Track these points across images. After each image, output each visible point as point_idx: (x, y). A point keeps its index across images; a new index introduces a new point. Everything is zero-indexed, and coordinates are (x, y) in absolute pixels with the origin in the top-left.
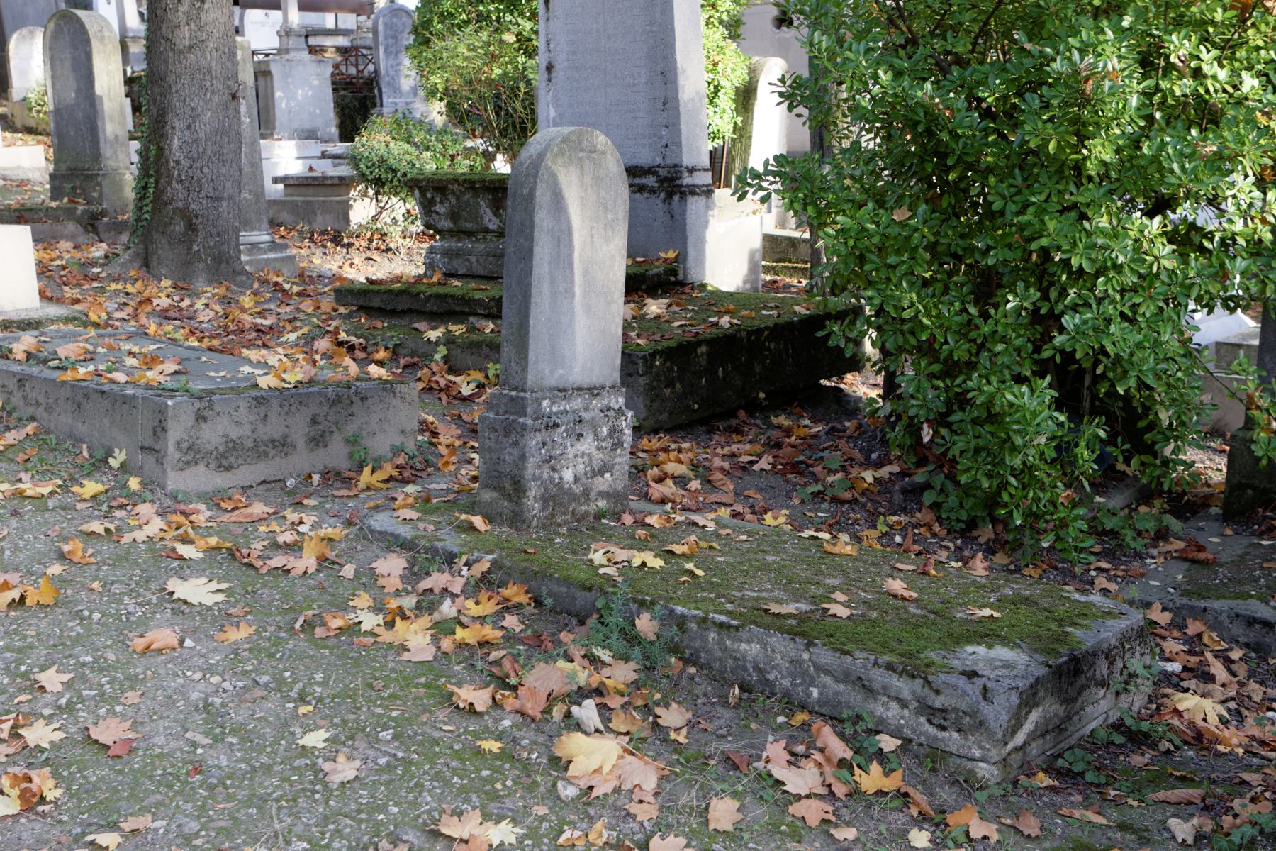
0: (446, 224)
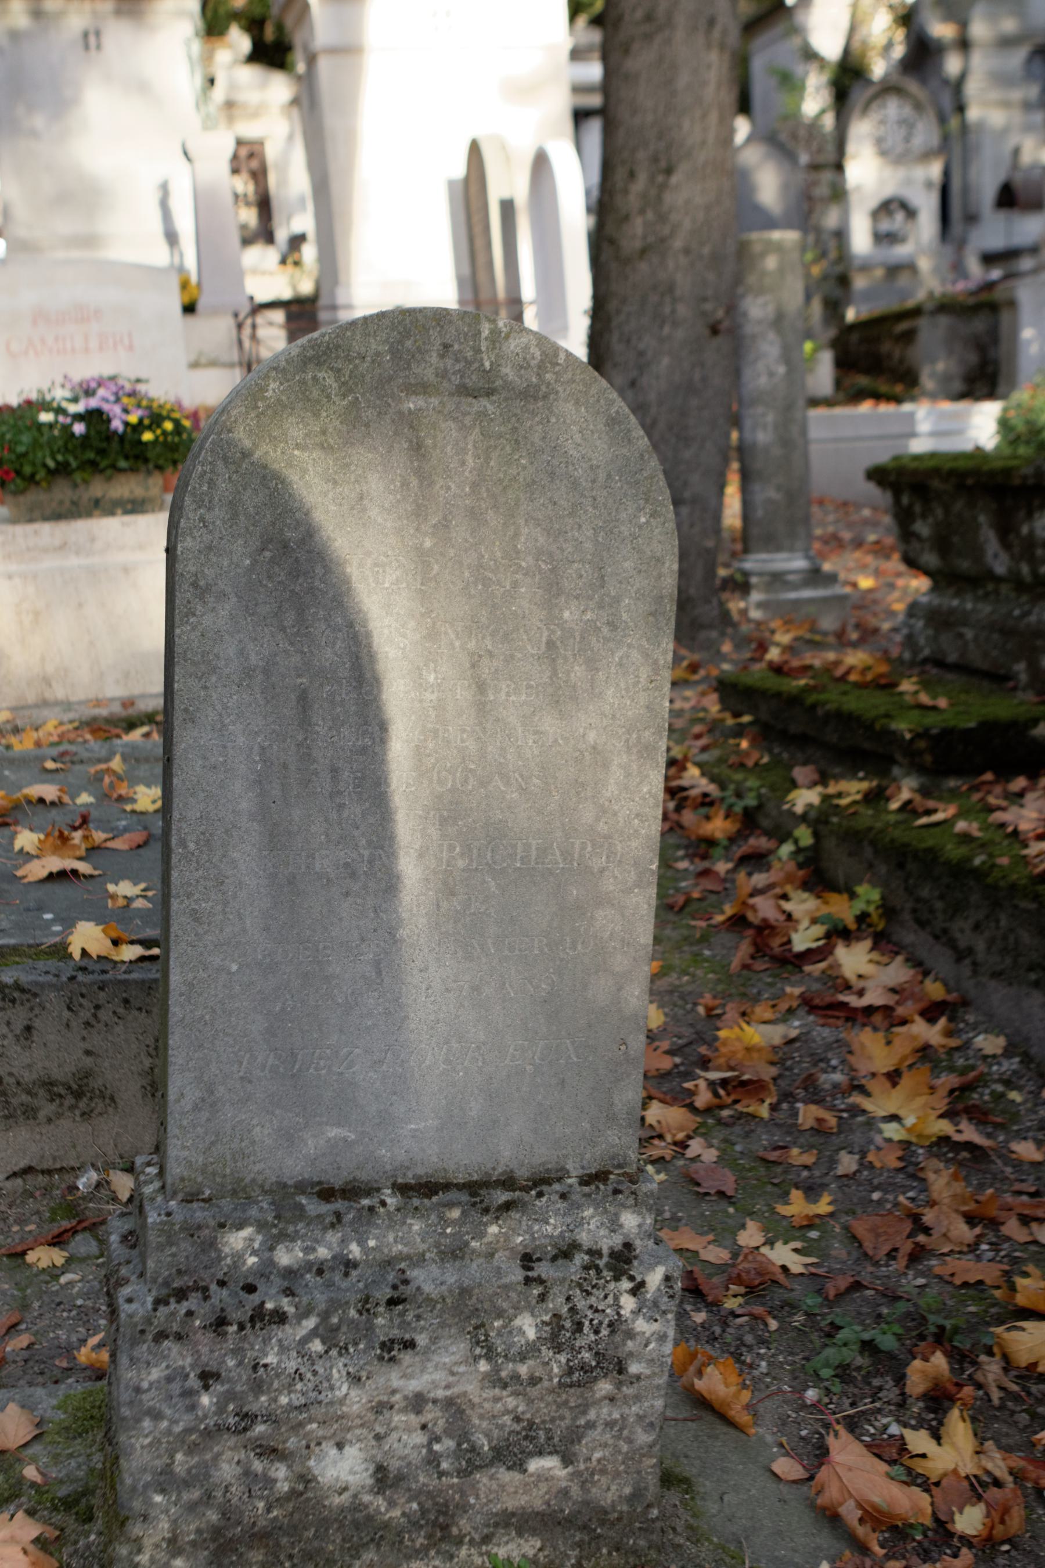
0: (931, 559)
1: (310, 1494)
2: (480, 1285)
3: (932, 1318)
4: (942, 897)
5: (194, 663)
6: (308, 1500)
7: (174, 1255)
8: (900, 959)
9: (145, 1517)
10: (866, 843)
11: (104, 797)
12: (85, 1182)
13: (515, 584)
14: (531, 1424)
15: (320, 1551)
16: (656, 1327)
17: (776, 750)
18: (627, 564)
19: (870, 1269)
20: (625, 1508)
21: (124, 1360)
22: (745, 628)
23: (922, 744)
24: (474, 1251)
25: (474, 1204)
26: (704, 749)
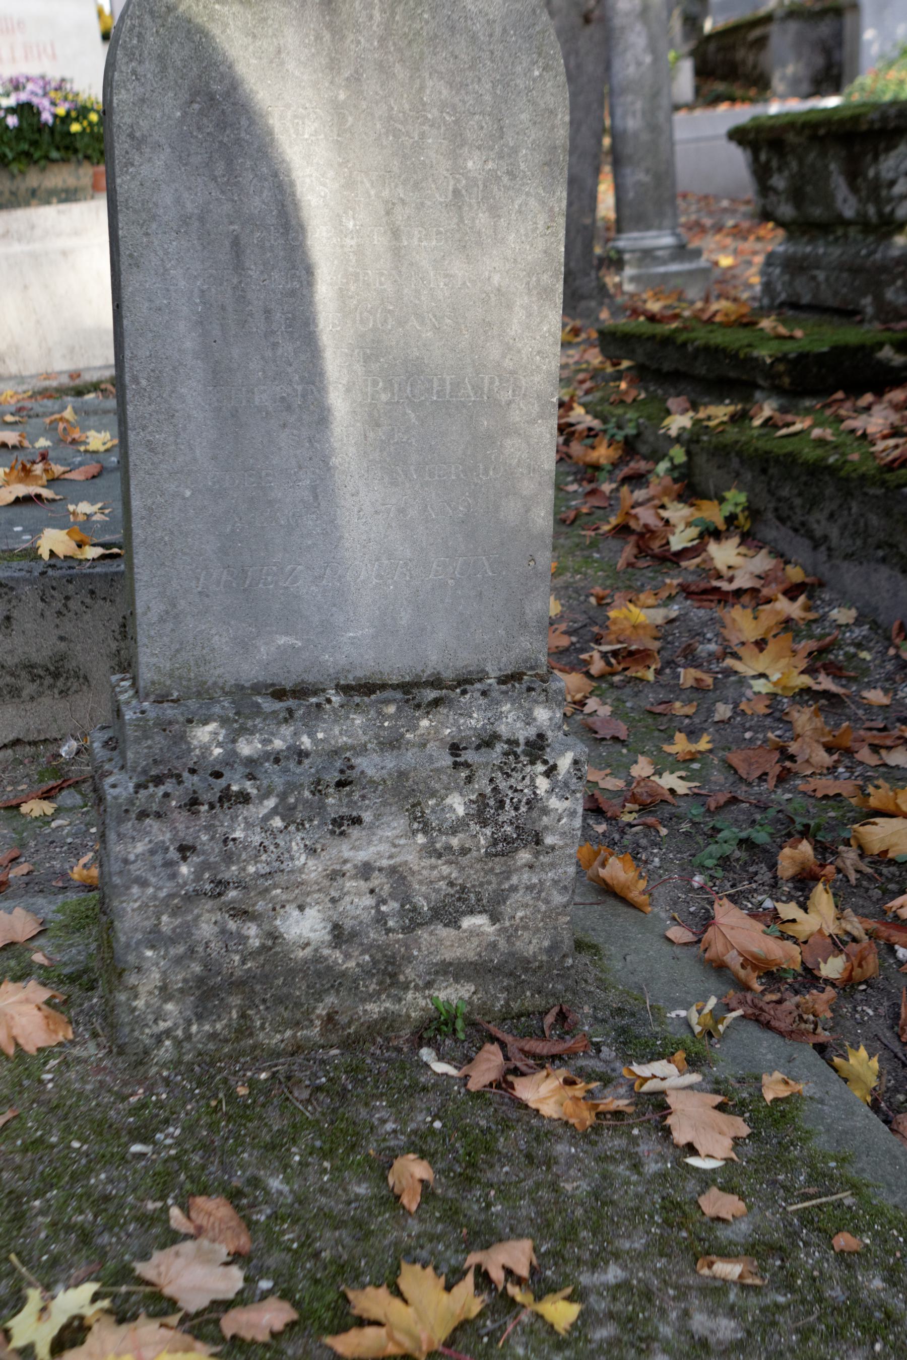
0: (786, 210)
1: (278, 949)
2: (415, 769)
3: (798, 820)
4: (800, 494)
5: (135, 211)
6: (277, 953)
7: (149, 747)
8: (764, 552)
9: (139, 969)
10: (733, 454)
11: (59, 442)
12: (67, 749)
13: (423, 135)
14: (463, 888)
15: (288, 996)
16: (567, 804)
17: (652, 388)
18: (523, 116)
19: (744, 788)
20: (545, 958)
21: (112, 836)
22: (619, 300)
23: (781, 367)
24: (408, 742)
25: (407, 701)
26: (588, 392)
